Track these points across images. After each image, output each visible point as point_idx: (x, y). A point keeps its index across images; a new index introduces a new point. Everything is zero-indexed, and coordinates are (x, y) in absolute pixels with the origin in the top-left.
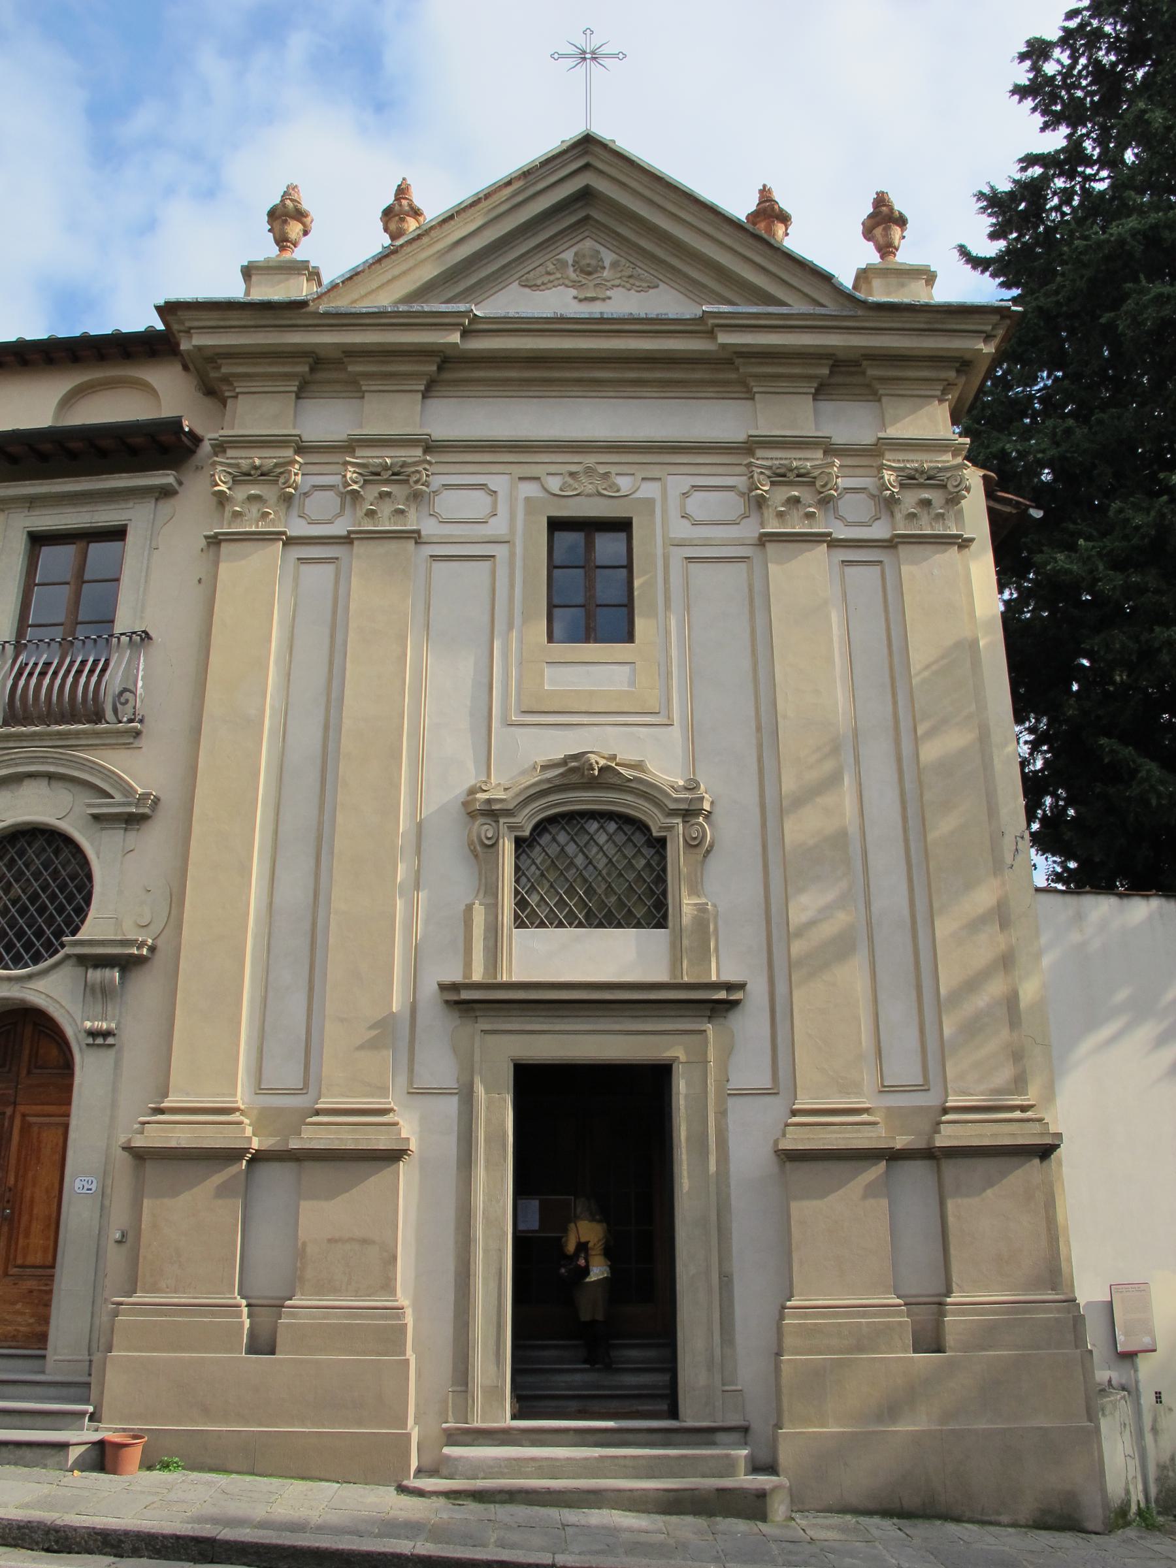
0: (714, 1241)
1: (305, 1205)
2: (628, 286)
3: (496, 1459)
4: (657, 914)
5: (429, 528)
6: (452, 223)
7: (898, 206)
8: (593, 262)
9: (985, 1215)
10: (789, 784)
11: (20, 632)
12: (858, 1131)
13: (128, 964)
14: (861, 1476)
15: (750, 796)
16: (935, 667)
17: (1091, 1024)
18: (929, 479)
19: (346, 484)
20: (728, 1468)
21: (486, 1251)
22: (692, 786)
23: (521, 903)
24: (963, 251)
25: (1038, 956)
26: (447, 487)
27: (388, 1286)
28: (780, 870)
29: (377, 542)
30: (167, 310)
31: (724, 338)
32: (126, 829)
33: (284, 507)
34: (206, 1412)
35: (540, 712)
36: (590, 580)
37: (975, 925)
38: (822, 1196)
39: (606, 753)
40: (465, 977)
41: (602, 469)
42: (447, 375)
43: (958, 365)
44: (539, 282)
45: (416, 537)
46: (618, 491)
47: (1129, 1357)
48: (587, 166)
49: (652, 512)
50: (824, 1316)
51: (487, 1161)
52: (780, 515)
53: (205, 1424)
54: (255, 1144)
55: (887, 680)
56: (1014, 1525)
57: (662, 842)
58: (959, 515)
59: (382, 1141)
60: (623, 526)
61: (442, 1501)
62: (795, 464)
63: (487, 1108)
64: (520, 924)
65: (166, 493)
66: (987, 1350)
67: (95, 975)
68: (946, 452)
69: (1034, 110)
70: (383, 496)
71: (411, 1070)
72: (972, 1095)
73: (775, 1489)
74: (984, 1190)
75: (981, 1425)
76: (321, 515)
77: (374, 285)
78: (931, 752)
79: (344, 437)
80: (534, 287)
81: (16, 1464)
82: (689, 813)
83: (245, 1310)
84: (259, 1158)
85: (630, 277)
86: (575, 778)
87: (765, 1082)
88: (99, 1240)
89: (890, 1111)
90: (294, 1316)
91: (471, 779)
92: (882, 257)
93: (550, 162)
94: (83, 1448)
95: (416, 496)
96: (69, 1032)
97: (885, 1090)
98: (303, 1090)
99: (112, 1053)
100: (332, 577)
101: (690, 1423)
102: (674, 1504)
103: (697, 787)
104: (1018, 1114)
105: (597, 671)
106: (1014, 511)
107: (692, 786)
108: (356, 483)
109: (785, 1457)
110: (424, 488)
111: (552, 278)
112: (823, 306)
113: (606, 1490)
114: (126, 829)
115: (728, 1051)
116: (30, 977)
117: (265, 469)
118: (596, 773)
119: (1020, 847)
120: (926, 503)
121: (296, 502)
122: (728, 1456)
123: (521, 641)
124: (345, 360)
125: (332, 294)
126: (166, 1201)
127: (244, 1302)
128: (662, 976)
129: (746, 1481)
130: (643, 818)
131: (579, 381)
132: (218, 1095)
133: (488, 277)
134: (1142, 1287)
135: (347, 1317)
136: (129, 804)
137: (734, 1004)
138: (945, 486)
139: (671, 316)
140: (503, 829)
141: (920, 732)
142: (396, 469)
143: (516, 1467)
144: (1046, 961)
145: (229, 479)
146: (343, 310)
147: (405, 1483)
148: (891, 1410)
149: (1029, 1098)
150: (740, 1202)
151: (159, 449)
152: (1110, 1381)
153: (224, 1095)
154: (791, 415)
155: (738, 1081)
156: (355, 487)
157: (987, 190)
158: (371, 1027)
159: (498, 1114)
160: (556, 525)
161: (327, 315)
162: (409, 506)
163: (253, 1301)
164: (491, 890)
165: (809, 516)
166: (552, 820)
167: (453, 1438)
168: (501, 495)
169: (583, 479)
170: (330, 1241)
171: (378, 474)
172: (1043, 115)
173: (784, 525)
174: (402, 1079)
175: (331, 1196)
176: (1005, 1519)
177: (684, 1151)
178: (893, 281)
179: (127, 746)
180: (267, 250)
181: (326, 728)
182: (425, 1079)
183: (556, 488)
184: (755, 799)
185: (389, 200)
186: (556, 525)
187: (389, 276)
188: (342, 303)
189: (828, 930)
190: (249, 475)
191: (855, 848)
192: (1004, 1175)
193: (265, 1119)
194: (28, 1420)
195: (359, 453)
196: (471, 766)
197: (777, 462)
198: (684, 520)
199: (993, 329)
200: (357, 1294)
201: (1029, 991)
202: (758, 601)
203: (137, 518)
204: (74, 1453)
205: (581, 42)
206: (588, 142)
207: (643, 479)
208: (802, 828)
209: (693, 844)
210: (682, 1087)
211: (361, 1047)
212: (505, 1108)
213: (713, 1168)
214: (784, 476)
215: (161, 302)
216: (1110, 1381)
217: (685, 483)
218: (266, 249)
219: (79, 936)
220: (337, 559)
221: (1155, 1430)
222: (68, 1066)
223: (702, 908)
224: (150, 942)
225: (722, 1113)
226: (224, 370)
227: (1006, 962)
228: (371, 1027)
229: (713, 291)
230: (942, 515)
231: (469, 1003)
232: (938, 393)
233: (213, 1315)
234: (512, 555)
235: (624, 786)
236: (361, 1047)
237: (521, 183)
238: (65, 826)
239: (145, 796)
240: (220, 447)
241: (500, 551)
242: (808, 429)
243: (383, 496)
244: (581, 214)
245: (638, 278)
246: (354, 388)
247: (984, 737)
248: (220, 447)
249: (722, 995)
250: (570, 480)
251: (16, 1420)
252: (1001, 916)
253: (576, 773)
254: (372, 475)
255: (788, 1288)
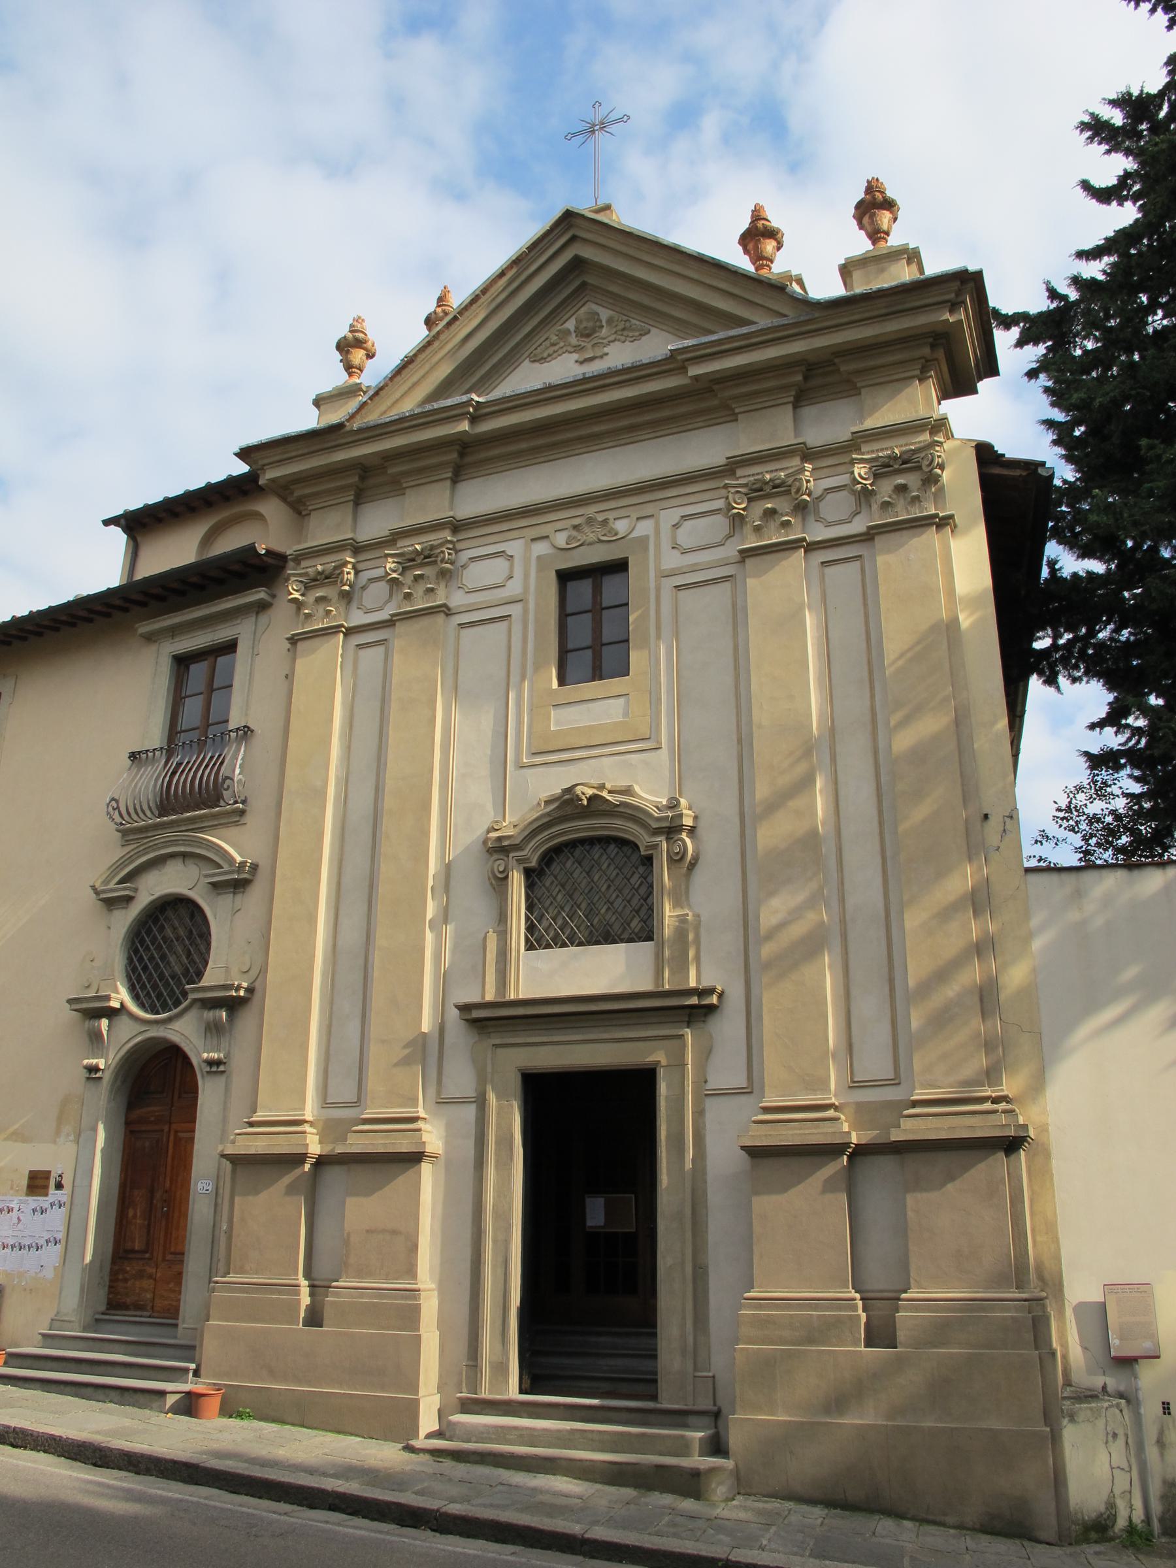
0: (689, 1235)
1: (910, 1199)
2: (623, 338)
3: (485, 1426)
4: (642, 929)
5: (457, 599)
6: (458, 323)
7: (775, 222)
8: (590, 324)
9: (946, 1212)
10: (762, 791)
11: (171, 739)
12: (817, 1127)
13: (234, 1005)
14: (808, 1463)
15: (730, 807)
16: (909, 655)
17: (1091, 1007)
18: (904, 463)
19: (388, 574)
20: (683, 1449)
21: (495, 1241)
22: (673, 805)
23: (530, 928)
24: (1086, 186)
25: (1029, 937)
26: (473, 559)
27: (411, 1271)
28: (756, 874)
29: (414, 620)
30: (244, 454)
31: (694, 371)
32: (234, 893)
33: (344, 603)
34: (273, 1375)
35: (548, 751)
36: (591, 623)
37: (947, 913)
38: (785, 1189)
39: (595, 782)
40: (657, 985)
41: (600, 517)
42: (468, 459)
43: (931, 340)
44: (545, 355)
45: (445, 610)
46: (616, 534)
47: (1127, 1363)
48: (574, 238)
49: (646, 549)
50: (777, 1307)
51: (497, 1161)
52: (757, 529)
53: (271, 1383)
54: (854, 1140)
55: (866, 674)
56: (960, 1527)
57: (648, 861)
58: (940, 495)
59: (403, 1145)
60: (620, 567)
61: (427, 1457)
62: (768, 477)
63: (498, 1114)
64: (530, 947)
65: (262, 607)
66: (936, 1347)
67: (209, 1015)
68: (924, 431)
69: (1153, 11)
70: (417, 578)
71: (439, 1082)
72: (939, 1087)
73: (712, 1470)
74: (943, 1185)
75: (928, 1423)
76: (375, 605)
77: (398, 395)
78: (903, 741)
79: (723, 461)
80: (542, 360)
81: (134, 1406)
82: (672, 830)
83: (860, 1303)
84: (861, 1151)
85: (624, 329)
86: (569, 810)
87: (740, 1081)
88: (214, 1231)
89: (860, 1107)
90: (337, 1295)
91: (488, 816)
92: (874, 243)
93: (536, 246)
94: (178, 1396)
95: (444, 574)
96: (195, 1061)
97: (856, 1085)
98: (895, 1082)
99: (223, 1078)
100: (382, 657)
101: (665, 1405)
102: (616, 1475)
103: (678, 804)
104: (988, 1106)
105: (601, 707)
106: (1024, 474)
107: (673, 805)
108: (394, 571)
109: (735, 1439)
110: (448, 565)
111: (556, 348)
112: (785, 316)
113: (560, 1459)
114: (234, 893)
115: (706, 1053)
116: (170, 1020)
117: (327, 573)
118: (585, 802)
119: (1008, 827)
120: (902, 489)
121: (356, 596)
122: (683, 1437)
123: (531, 690)
124: (836, 360)
125: (363, 412)
126: (250, 1198)
127: (858, 1296)
128: (646, 985)
129: (698, 1461)
130: (632, 839)
131: (581, 439)
132: (292, 1110)
133: (500, 362)
134: (1142, 1290)
135: (376, 1297)
136: (231, 872)
137: (711, 1008)
138: (919, 468)
139: (645, 361)
140: (512, 862)
141: (892, 723)
142: (427, 553)
143: (502, 1434)
144: (1037, 944)
145: (301, 586)
146: (372, 424)
147: (412, 1442)
148: (838, 1403)
149: (1008, 1087)
150: (716, 1197)
151: (255, 572)
152: (1104, 1388)
153: (295, 1110)
154: (774, 428)
155: (716, 1081)
156: (394, 575)
157: (1087, 119)
158: (405, 1047)
159: (509, 1120)
160: (565, 577)
161: (360, 430)
162: (438, 584)
163: (316, 1283)
164: (502, 918)
165: (786, 524)
166: (557, 850)
167: (467, 1406)
168: (516, 560)
169: (586, 529)
170: (367, 1231)
171: (413, 560)
172: (1166, 13)
173: (761, 538)
174: (432, 1091)
175: (369, 1192)
176: (950, 1520)
177: (664, 1149)
178: (872, 268)
179: (236, 823)
180: (861, 245)
181: (377, 789)
182: (451, 1091)
183: (558, 543)
184: (736, 809)
185: (861, 195)
186: (565, 577)
187: (409, 384)
188: (373, 417)
189: (798, 930)
190: (315, 580)
191: (828, 849)
192: (966, 1168)
193: (331, 1129)
194: (152, 1373)
195: (739, 473)
196: (489, 807)
197: (752, 479)
198: (675, 551)
199: (957, 295)
200: (387, 1278)
201: (1016, 976)
202: (737, 615)
203: (242, 630)
204: (171, 1400)
205: (590, 117)
206: (568, 217)
207: (532, 540)
208: (772, 834)
209: (677, 859)
210: (663, 1089)
211: (396, 1065)
212: (512, 1113)
213: (689, 1165)
214: (761, 490)
215: (237, 450)
216: (1104, 1388)
217: (674, 515)
218: (860, 244)
219: (204, 983)
220: (860, 556)
221: (1161, 1443)
222: (193, 1091)
223: (682, 919)
224: (245, 985)
225: (699, 1113)
226: (296, 494)
227: (982, 948)
228: (405, 1047)
229: (695, 326)
230: (917, 497)
231: (491, 1021)
232: (918, 372)
233: (280, 1293)
234: (526, 611)
235: (612, 811)
236: (396, 1065)
237: (514, 270)
238: (192, 894)
239: (243, 864)
240: (299, 558)
241: (515, 610)
242: (787, 438)
243: (417, 578)
244: (577, 283)
245: (630, 329)
246: (397, 488)
247: (961, 721)
248: (299, 558)
249: (694, 1001)
250: (575, 533)
251: (139, 1372)
252: (979, 900)
253: (568, 805)
254: (408, 562)
255: (762, 1280)
